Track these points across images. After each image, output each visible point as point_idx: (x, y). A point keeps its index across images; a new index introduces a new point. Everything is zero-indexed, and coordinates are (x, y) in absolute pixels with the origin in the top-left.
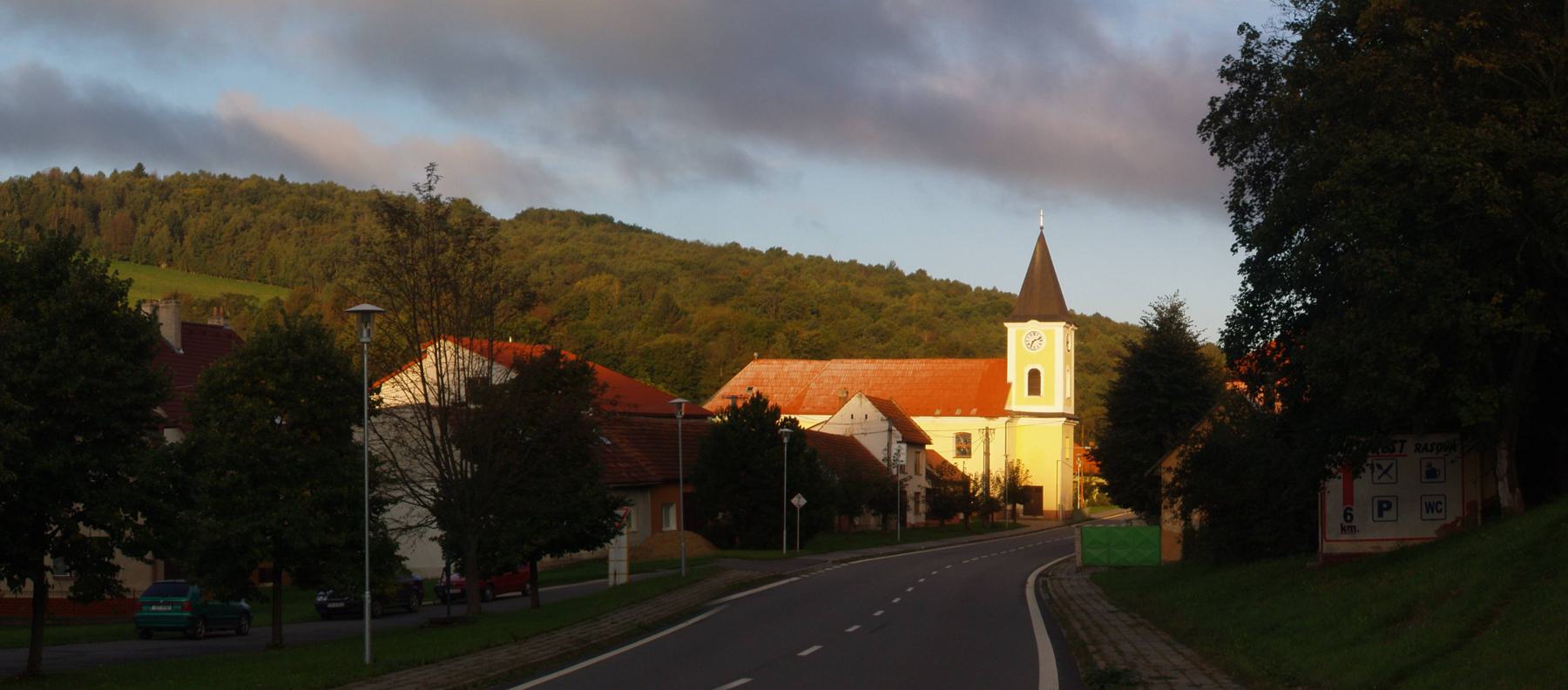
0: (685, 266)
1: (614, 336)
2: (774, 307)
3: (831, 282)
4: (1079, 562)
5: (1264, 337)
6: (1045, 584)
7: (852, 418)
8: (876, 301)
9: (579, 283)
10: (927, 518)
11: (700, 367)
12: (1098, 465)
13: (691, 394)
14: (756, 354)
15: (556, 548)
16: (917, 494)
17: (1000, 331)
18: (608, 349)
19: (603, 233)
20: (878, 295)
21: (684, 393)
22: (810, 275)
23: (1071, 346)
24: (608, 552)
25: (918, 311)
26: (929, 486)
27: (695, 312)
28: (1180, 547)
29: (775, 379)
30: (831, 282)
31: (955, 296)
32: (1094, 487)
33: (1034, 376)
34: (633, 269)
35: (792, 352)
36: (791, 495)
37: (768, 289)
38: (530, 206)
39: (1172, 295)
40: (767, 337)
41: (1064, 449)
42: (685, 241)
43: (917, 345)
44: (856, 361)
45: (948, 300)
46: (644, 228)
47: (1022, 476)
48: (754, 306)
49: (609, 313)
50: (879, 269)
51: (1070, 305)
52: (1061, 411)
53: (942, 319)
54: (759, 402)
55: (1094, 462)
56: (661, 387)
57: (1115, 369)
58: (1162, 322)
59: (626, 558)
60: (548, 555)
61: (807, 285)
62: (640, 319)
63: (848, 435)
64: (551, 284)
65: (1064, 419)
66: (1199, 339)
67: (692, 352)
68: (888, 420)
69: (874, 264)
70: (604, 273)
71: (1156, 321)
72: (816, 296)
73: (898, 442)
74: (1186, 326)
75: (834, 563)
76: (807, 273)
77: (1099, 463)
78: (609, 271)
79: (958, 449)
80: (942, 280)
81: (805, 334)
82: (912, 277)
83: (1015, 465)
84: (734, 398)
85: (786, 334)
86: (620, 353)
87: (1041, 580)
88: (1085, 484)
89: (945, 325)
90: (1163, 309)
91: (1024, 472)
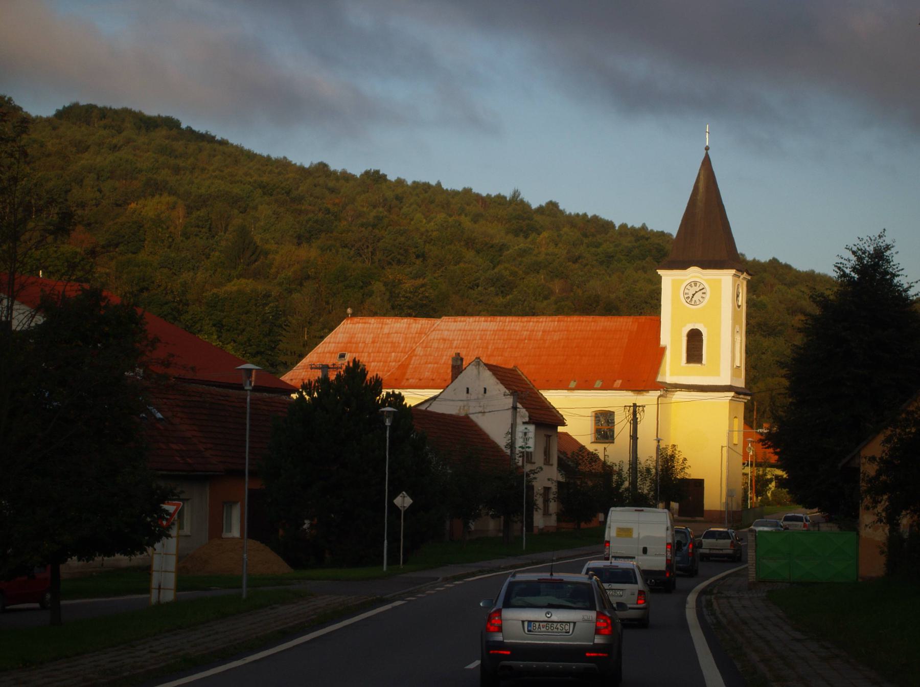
0: (267, 190)
1: (175, 277)
2: (370, 249)
3: (441, 217)
4: (752, 576)
5: (816, 299)
6: (709, 604)
7: (468, 392)
8: (496, 241)
9: (133, 205)
10: (559, 520)
11: (280, 326)
12: (776, 453)
13: (267, 361)
14: (349, 311)
15: (86, 550)
16: (547, 489)
17: (650, 281)
18: (166, 294)
19: (167, 142)
20: (497, 233)
21: (258, 358)
22: (414, 206)
23: (742, 300)
24: (152, 558)
25: (547, 254)
26: (561, 479)
27: (277, 252)
28: (883, 559)
29: (373, 342)
30: (441, 217)
31: (594, 236)
32: (770, 481)
33: (695, 338)
34: (203, 191)
35: (393, 308)
36: (394, 494)
37: (362, 225)
38: (74, 100)
39: (877, 236)
40: (362, 288)
41: (731, 431)
42: (269, 158)
43: (546, 298)
44: (471, 319)
45: (586, 241)
46: (218, 138)
47: (678, 466)
48: (346, 246)
49: (169, 247)
50: (500, 199)
51: (741, 248)
52: (728, 383)
53: (577, 266)
54: (356, 371)
55: (771, 450)
56: (229, 348)
57: (800, 330)
58: (861, 269)
59: (173, 569)
60: (75, 558)
61: (412, 220)
62: (208, 257)
63: (463, 414)
64: (97, 205)
65: (732, 394)
66: (911, 292)
67: (272, 305)
68: (512, 394)
69: (493, 194)
70: (166, 194)
71: (854, 269)
72: (422, 234)
73: (524, 423)
74: (894, 275)
75: (446, 580)
76: (411, 204)
77: (778, 450)
78: (172, 192)
79: (598, 431)
80: (578, 215)
81: (408, 285)
82: (541, 210)
83: (669, 453)
84: (325, 368)
85: (386, 284)
86: (181, 301)
87: (704, 598)
88: (758, 476)
89: (580, 273)
90: (864, 253)
91: (681, 461)
